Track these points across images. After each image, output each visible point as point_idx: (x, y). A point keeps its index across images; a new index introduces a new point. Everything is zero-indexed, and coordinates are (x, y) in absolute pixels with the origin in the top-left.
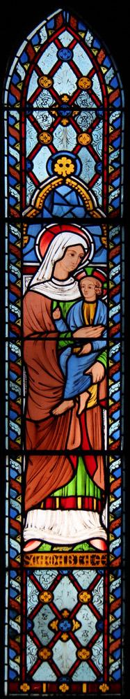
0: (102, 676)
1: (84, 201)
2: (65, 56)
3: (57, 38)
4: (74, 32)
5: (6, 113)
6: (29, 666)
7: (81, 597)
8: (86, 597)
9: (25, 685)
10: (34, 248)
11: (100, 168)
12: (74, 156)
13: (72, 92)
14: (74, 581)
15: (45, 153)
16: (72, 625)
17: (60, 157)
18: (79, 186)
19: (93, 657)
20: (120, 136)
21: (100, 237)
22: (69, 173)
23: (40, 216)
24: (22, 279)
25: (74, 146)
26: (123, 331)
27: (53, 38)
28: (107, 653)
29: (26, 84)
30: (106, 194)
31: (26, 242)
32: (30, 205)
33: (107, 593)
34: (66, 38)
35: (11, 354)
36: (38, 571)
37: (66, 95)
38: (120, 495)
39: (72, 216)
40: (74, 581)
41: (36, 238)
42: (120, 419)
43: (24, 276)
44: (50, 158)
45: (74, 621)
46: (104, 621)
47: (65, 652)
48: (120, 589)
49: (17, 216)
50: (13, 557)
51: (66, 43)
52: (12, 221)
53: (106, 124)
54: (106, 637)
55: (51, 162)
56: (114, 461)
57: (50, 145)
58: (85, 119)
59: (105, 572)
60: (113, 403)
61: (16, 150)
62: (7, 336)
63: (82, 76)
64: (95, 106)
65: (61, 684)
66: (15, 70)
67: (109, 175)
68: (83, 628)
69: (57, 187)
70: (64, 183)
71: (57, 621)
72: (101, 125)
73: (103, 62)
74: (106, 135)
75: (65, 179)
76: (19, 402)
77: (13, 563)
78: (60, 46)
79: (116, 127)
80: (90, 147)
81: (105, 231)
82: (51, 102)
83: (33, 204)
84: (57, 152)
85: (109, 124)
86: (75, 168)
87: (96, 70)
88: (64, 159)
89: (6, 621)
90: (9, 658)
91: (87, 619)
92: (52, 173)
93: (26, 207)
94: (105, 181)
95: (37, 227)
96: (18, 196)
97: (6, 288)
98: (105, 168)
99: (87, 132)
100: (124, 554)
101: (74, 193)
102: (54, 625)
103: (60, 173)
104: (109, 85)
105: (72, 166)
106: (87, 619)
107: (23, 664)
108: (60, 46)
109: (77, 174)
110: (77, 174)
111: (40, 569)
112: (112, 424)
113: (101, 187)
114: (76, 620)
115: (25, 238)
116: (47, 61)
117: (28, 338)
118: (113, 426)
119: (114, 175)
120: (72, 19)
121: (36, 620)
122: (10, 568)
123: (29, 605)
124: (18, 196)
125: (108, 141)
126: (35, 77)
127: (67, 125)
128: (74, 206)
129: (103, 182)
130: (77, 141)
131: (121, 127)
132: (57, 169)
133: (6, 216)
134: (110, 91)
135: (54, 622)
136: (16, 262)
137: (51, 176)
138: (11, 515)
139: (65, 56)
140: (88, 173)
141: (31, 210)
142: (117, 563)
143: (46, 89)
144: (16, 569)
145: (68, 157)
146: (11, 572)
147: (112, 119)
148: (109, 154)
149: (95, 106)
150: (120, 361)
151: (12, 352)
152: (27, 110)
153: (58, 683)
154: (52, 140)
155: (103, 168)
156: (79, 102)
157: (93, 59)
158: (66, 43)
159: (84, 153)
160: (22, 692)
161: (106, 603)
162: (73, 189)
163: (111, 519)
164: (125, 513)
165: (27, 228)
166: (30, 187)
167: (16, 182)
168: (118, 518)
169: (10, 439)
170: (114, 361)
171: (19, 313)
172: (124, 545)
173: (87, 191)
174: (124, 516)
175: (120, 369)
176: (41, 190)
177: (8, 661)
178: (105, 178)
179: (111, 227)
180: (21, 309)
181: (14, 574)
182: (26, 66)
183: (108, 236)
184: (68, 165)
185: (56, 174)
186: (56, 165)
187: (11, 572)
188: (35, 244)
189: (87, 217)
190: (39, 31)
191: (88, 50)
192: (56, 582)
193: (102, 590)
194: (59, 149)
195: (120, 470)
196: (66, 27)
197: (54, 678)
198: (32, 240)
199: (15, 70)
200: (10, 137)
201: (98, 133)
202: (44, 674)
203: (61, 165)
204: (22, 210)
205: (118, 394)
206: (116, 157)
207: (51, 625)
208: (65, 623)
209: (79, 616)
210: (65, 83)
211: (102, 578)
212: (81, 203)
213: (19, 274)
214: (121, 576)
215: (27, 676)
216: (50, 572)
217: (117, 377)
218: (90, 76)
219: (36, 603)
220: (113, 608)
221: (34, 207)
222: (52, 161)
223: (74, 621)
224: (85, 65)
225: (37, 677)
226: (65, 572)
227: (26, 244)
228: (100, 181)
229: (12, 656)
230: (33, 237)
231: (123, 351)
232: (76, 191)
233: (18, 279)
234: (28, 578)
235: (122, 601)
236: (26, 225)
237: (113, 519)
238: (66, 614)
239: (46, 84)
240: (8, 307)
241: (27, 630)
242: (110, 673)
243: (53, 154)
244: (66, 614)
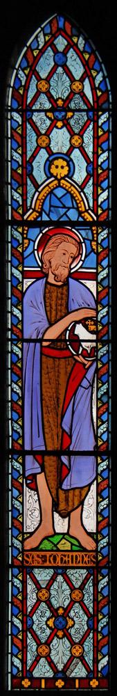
0: (92, 673)
1: (77, 204)
2: (61, 62)
3: (52, 43)
4: (68, 38)
5: (9, 114)
6: (29, 662)
7: (74, 651)
8: (77, 141)
9: (27, 680)
10: (33, 252)
11: (90, 169)
12: (67, 157)
13: (66, 95)
14: (68, 581)
15: (43, 154)
16: (67, 623)
17: (57, 159)
18: (72, 187)
19: (84, 145)
20: (108, 294)
21: (91, 241)
22: (63, 175)
23: (39, 219)
24: (22, 282)
25: (68, 148)
26: (110, 411)
27: (49, 42)
28: (97, 649)
29: (26, 88)
30: (96, 196)
31: (26, 245)
32: (31, 208)
33: (96, 592)
34: (61, 43)
35: (13, 393)
36: (36, 570)
37: (61, 98)
38: (107, 612)
39: (67, 219)
40: (68, 581)
41: (34, 242)
42: (108, 266)
43: (25, 280)
44: (48, 160)
45: (67, 618)
46: (94, 619)
47: (60, 651)
48: (107, 240)
49: (20, 219)
50: (15, 556)
51: (61, 48)
52: (15, 223)
53: (96, 125)
54: (96, 634)
55: (48, 163)
56: (102, 271)
57: (48, 148)
58: (77, 120)
59: (94, 572)
60: (100, 93)
61: (18, 658)
62: (10, 337)
63: (75, 80)
64: (86, 108)
65: (57, 681)
66: (12, 274)
67: (98, 175)
68: (76, 626)
69: (54, 189)
70: (59, 186)
71: (54, 619)
72: (91, 127)
73: (93, 65)
74: (96, 137)
75: (59, 180)
76: (21, 481)
77: (16, 445)
78: (56, 51)
79: (105, 362)
80: (81, 603)
81: (95, 235)
82: (48, 106)
83: (33, 207)
84: (53, 154)
85: (98, 127)
86: (69, 171)
87: (87, 75)
88: (60, 160)
89: (10, 579)
90: (12, 614)
91: (79, 620)
92: (49, 175)
93: (28, 211)
94: (95, 183)
95: (37, 230)
96: (19, 391)
97: (9, 330)
98: (95, 169)
99: (78, 134)
100: (110, 216)
101: (69, 195)
102: (51, 623)
103: (55, 174)
104: (99, 88)
105: (67, 168)
106: (79, 620)
107: (24, 661)
108: (56, 51)
109: (70, 176)
110: (70, 176)
111: (38, 567)
112: (100, 463)
113: (91, 188)
114: (70, 618)
115: (26, 241)
116: (44, 68)
117: (30, 453)
118: (102, 389)
119: (102, 602)
120: (67, 24)
121: (34, 618)
122: (13, 566)
123: (28, 604)
124: (19, 391)
125: (98, 608)
126: (34, 81)
127: (58, 608)
128: (69, 208)
129: (93, 184)
130: (70, 143)
131: (108, 247)
132: (54, 170)
133: (9, 689)
134: (99, 94)
135: (51, 620)
136: (17, 188)
137: (48, 178)
138: (13, 417)
139: (61, 62)
140: (80, 175)
141: (32, 213)
142: (104, 563)
143: (43, 93)
144: (18, 567)
145: (64, 159)
146: (14, 569)
147: (101, 122)
148: (98, 156)
149: (86, 108)
150: (108, 478)
151: (14, 276)
152: (26, 111)
153: (55, 679)
154: (50, 652)
155: (93, 169)
156: (72, 105)
157: (85, 64)
158: (61, 48)
159: (76, 154)
160: (22, 686)
161: (95, 601)
162: (68, 192)
163: (100, 289)
164: (111, 504)
165: (27, 231)
166: (31, 188)
167: (17, 378)
168: (105, 151)
169: (12, 208)
170: (102, 247)
171: (19, 315)
172: (110, 442)
173: (79, 193)
174: (110, 363)
175: (107, 409)
176: (40, 193)
177: (12, 578)
178: (96, 178)
179: (100, 230)
180: (22, 312)
181: (16, 571)
182: (25, 71)
183: (97, 241)
184: (62, 167)
185: (52, 175)
186: (53, 166)
187: (14, 569)
188: (34, 250)
189: (81, 219)
190: (37, 37)
191: (80, 54)
192: (53, 579)
193: (91, 588)
194: (54, 151)
195: (107, 471)
196: (60, 31)
197: (50, 674)
198: (32, 243)
199: (12, 274)
200: (14, 529)
201: (88, 136)
202: (43, 671)
203: (57, 167)
204: (24, 213)
205: (107, 589)
206: (105, 391)
207: (48, 623)
208: (60, 112)
209: (72, 614)
210: (60, 88)
211: (92, 577)
212: (75, 206)
213: (20, 277)
214: (108, 654)
215: (27, 673)
216: (47, 571)
217: (105, 650)
218: (82, 80)
219: (35, 601)
220: (101, 644)
221: (34, 210)
222: (49, 163)
223: (67, 618)
224: (78, 71)
225: (36, 674)
226: (60, 571)
227: (27, 248)
228: (91, 182)
229: (15, 613)
230: (32, 240)
231: (110, 430)
232: (72, 196)
233: (20, 282)
234: (28, 577)
235: (109, 251)
236: (26, 228)
237: (101, 327)
238: (59, 124)
239: (44, 597)
240: (11, 581)
241: (28, 628)
242: (99, 204)
243: (50, 156)
244: (61, 611)
